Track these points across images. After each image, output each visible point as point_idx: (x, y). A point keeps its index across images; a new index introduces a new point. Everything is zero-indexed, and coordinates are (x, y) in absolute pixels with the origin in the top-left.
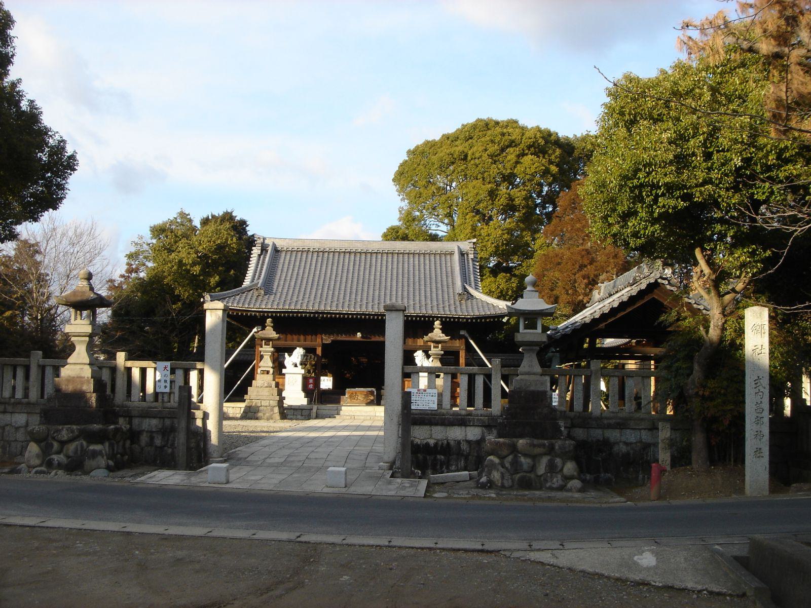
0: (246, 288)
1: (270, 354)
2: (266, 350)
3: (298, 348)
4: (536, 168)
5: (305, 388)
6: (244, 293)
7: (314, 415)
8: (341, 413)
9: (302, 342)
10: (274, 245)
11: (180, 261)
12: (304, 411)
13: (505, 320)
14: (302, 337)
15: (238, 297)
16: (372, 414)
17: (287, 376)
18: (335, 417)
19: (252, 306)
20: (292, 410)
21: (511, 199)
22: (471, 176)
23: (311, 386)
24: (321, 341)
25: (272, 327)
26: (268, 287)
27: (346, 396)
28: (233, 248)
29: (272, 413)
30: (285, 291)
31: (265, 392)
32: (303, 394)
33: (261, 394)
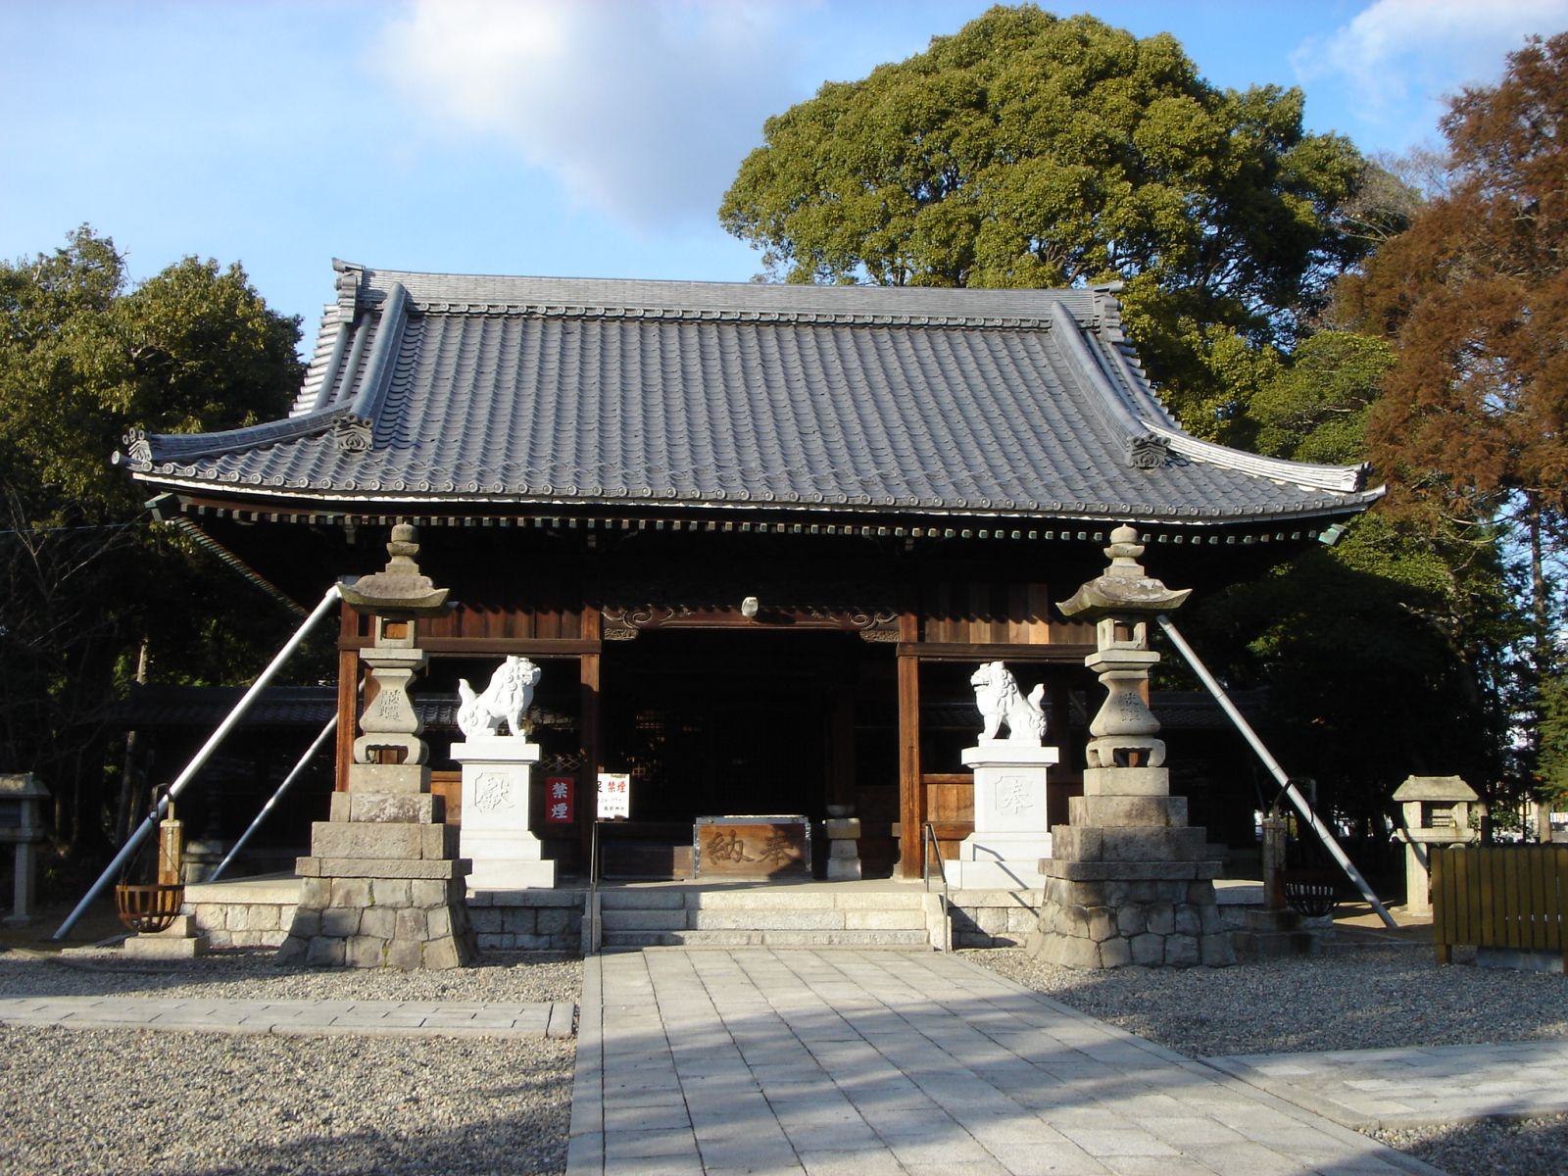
0: (300, 424)
1: (408, 673)
2: (394, 653)
3: (511, 659)
4: (1200, 129)
5: (539, 822)
6: (292, 442)
7: (592, 933)
8: (703, 920)
9: (523, 638)
10: (403, 294)
11: (64, 364)
12: (544, 916)
13: (1328, 537)
14: (522, 620)
15: (266, 456)
16: (832, 920)
17: (467, 771)
18: (679, 942)
19: (325, 481)
20: (496, 916)
21: (1146, 213)
22: (1009, 147)
23: (560, 811)
24: (595, 632)
25: (416, 558)
26: (386, 418)
27: (697, 846)
28: (254, 333)
29: (422, 937)
30: (456, 433)
31: (391, 843)
32: (535, 845)
33: (370, 852)
